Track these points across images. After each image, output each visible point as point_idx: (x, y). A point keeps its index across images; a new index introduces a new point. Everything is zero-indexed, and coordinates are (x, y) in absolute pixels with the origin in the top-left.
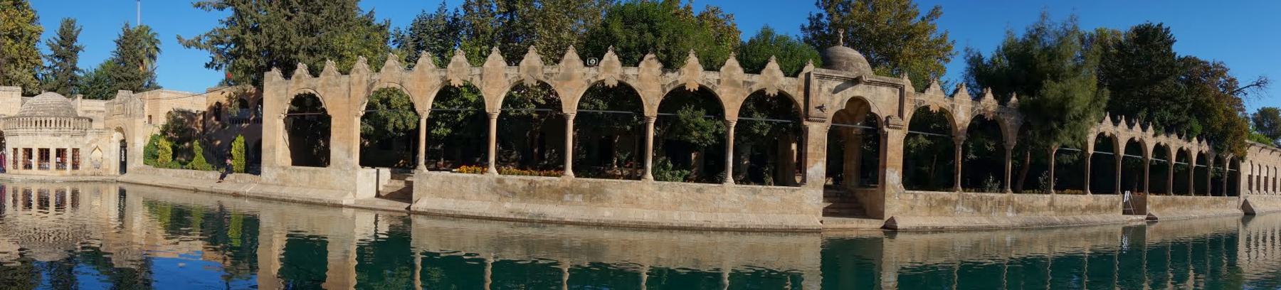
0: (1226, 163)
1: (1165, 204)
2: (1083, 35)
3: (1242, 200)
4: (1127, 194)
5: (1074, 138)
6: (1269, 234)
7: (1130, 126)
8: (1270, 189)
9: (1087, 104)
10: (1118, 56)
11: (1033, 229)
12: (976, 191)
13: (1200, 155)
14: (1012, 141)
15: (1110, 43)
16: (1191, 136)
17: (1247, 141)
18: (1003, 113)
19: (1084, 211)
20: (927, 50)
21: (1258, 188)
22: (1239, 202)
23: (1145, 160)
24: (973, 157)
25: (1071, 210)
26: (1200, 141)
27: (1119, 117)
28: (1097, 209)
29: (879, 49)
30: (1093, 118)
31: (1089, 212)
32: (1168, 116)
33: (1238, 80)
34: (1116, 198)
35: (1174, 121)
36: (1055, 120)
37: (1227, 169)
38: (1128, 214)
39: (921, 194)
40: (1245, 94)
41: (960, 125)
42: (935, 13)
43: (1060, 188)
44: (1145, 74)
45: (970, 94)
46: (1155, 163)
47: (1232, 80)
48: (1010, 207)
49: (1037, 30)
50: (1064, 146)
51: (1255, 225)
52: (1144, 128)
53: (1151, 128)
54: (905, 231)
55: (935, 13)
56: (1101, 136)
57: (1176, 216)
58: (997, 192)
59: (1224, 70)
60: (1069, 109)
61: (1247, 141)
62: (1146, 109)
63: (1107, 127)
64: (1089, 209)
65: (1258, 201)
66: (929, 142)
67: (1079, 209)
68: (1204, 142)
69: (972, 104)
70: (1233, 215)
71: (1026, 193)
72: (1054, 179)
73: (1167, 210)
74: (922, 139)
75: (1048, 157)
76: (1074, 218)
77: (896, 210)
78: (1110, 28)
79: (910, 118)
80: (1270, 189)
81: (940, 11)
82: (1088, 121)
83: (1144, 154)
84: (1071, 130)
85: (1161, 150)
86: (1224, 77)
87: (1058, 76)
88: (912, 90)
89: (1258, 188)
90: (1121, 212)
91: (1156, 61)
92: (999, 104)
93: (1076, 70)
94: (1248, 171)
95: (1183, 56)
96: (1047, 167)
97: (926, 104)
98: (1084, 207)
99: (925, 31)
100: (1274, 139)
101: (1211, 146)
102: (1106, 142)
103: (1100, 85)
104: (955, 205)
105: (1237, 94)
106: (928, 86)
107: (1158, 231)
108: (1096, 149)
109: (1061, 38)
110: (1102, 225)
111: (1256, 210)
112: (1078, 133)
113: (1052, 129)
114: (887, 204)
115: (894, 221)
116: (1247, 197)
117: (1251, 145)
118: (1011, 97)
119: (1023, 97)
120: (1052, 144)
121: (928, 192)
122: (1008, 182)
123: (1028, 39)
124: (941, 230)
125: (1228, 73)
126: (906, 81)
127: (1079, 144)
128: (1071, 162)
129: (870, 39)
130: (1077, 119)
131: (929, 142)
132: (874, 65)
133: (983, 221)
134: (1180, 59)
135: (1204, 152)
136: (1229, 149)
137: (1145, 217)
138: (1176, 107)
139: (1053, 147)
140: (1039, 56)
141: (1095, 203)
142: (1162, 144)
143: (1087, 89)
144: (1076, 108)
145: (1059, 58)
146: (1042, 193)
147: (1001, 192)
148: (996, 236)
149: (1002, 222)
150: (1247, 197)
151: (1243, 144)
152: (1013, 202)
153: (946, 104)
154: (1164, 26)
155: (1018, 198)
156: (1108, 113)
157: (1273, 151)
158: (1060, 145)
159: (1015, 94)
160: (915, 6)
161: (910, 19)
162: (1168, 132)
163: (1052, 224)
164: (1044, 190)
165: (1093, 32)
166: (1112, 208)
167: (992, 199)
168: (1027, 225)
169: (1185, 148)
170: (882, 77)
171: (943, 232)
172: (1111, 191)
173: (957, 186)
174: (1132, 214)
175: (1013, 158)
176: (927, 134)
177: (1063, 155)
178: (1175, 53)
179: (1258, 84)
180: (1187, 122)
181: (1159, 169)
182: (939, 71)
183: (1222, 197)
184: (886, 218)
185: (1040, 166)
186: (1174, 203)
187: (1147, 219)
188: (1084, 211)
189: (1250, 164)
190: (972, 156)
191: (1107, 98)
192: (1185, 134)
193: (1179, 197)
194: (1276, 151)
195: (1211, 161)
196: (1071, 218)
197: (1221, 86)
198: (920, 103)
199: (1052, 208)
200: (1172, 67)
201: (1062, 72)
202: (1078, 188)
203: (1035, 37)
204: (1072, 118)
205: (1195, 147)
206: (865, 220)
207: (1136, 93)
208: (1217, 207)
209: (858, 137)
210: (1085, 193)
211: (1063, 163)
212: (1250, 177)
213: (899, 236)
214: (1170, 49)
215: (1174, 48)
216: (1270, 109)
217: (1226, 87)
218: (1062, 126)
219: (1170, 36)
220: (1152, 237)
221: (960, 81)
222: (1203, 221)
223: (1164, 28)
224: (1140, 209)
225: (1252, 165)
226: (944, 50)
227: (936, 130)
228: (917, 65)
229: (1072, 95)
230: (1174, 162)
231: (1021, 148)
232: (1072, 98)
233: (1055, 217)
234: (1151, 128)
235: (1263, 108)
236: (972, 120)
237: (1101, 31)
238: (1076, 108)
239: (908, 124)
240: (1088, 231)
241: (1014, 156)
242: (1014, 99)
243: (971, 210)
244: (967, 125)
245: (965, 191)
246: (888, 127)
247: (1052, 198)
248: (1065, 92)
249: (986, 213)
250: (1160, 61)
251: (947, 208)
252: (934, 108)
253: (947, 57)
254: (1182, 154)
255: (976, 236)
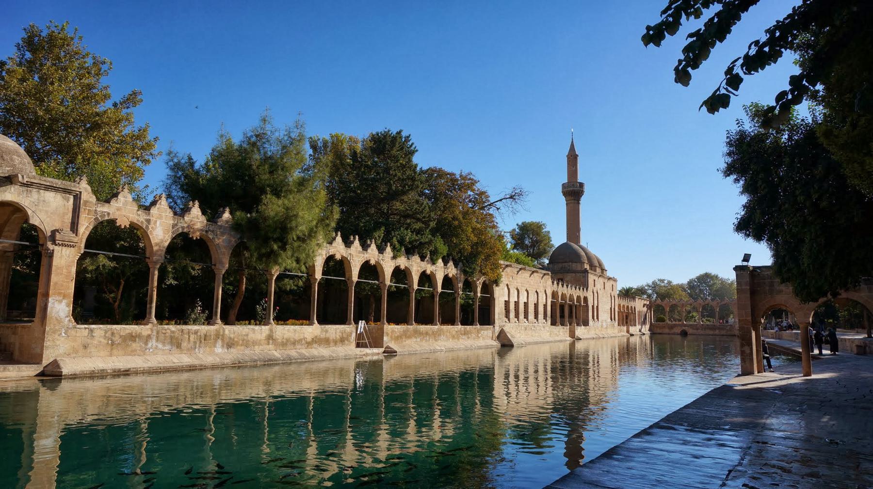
0: (477, 287)
1: (406, 335)
2: (316, 141)
3: (497, 329)
4: (362, 324)
5: (298, 261)
6: (531, 370)
7: (365, 247)
8: (531, 316)
9: (314, 223)
10: (353, 167)
11: (246, 367)
12: (176, 323)
13: (447, 281)
14: (223, 264)
15: (347, 152)
16: (435, 258)
17: (502, 262)
18: (213, 231)
19: (309, 344)
20: (118, 146)
21: (517, 316)
22: (493, 332)
23: (381, 285)
24: (174, 282)
25: (294, 343)
26: (446, 263)
27: (352, 237)
28: (326, 342)
29: (50, 138)
30: (321, 238)
31: (315, 345)
32: (409, 236)
33: (489, 193)
34: (348, 329)
35: (416, 241)
36: (275, 241)
37: (479, 295)
38: (362, 347)
39: (100, 330)
40: (498, 209)
41: (157, 244)
42: (132, 99)
43: (282, 318)
44: (383, 188)
45: (171, 207)
46: (393, 289)
47: (482, 193)
48: (220, 342)
49: (257, 136)
50: (286, 270)
51: (514, 358)
52: (381, 250)
53: (389, 249)
54: (74, 377)
55: (132, 99)
56: (330, 258)
57: (418, 348)
58: (204, 324)
59: (474, 182)
60: (291, 229)
61: (502, 262)
62: (383, 228)
63: (338, 248)
64: (316, 342)
65: (516, 331)
66: (113, 264)
67: (303, 342)
68: (451, 264)
69: (174, 219)
70: (487, 347)
71: (241, 324)
72: (274, 310)
73: (408, 342)
74: (103, 260)
75: (267, 282)
76: (297, 352)
77: (61, 351)
78: (347, 135)
79: (88, 233)
80: (531, 316)
81: (139, 97)
82: (314, 242)
83: (381, 280)
84: (294, 252)
85: (400, 274)
86: (473, 190)
87: (281, 191)
88: (93, 199)
89: (517, 316)
90: (354, 344)
91: (394, 173)
92: (207, 221)
93: (302, 183)
94: (503, 295)
95: (425, 168)
96: (265, 294)
97: (112, 217)
98: (309, 339)
99: (118, 122)
100: (536, 259)
101: (459, 268)
102: (335, 266)
103: (331, 201)
104: (147, 341)
105: (489, 210)
106: (116, 195)
107: (399, 366)
108: (324, 273)
109: (284, 147)
110: (346, 359)
111: (515, 341)
112: (303, 256)
113: (272, 251)
114: (47, 343)
115: (58, 366)
116: (504, 326)
117: (507, 266)
118: (223, 212)
119: (238, 213)
120: (272, 268)
121: (109, 326)
122: (216, 312)
123: (245, 146)
124: (126, 373)
125: (477, 187)
126: (84, 187)
127: (303, 268)
128: (295, 288)
129: (36, 122)
130: (302, 239)
131: (113, 264)
132: (37, 157)
133: (184, 359)
134: (422, 172)
135: (450, 275)
136: (480, 271)
137: (382, 350)
138: (418, 225)
139: (273, 272)
140: (258, 168)
141: (323, 336)
142: (402, 267)
143: (314, 206)
144: (300, 228)
145: (282, 169)
146: (260, 324)
147: (209, 324)
148: (200, 378)
149: (209, 360)
150: (504, 326)
151: (496, 266)
152: (223, 335)
153: (138, 217)
154: (404, 134)
155: (230, 330)
156: (339, 233)
157: (533, 272)
158: (282, 269)
159: (228, 210)
160: (106, 88)
161: (97, 102)
162: (409, 252)
163: (270, 360)
164: (261, 320)
165: (328, 138)
166: (343, 340)
167: (196, 332)
168: (239, 362)
169: (428, 272)
170: (49, 179)
171: (128, 375)
172: (342, 320)
173: (150, 317)
174: (367, 347)
175: (224, 282)
176: (111, 254)
177: (287, 280)
178: (417, 165)
179: (511, 197)
180: (430, 242)
181: (399, 296)
182: (134, 174)
183: (474, 326)
184: (45, 362)
185: (257, 293)
186: (417, 333)
187: (384, 352)
188: (309, 344)
189: (506, 288)
190: (171, 281)
191: (337, 216)
192: (429, 255)
193: (423, 328)
194: (537, 272)
195: (460, 285)
196: (293, 353)
197: (470, 201)
198: (103, 216)
199: (271, 342)
200: (413, 179)
201: (284, 186)
202: (303, 317)
203: (254, 144)
204: (295, 239)
205: (440, 270)
206: (10, 367)
207: (373, 209)
208: (468, 338)
209: (9, 254)
210: (311, 324)
211: (286, 290)
212: (507, 303)
213: (65, 386)
214: (410, 160)
215: (416, 159)
216: (532, 224)
217: (475, 202)
218: (283, 248)
219: (411, 146)
220: (390, 372)
221: (159, 192)
222: (450, 355)
223: (404, 136)
224: (376, 342)
225: (509, 289)
226: (142, 148)
227: (123, 249)
228: (104, 165)
229: (295, 213)
230: (416, 287)
231: (233, 274)
232: (296, 216)
233: (274, 352)
234: (389, 249)
235: (523, 223)
236: (174, 239)
237: (337, 136)
238: (300, 228)
239: (84, 241)
240: (315, 367)
241: (227, 281)
242: (227, 215)
243: (168, 347)
244: (166, 244)
245: (161, 324)
246: (54, 242)
247: (271, 330)
248: (287, 209)
249: (188, 350)
250: (399, 174)
251: (135, 346)
252: (123, 222)
253: (146, 157)
254: (426, 279)
255: (173, 378)
